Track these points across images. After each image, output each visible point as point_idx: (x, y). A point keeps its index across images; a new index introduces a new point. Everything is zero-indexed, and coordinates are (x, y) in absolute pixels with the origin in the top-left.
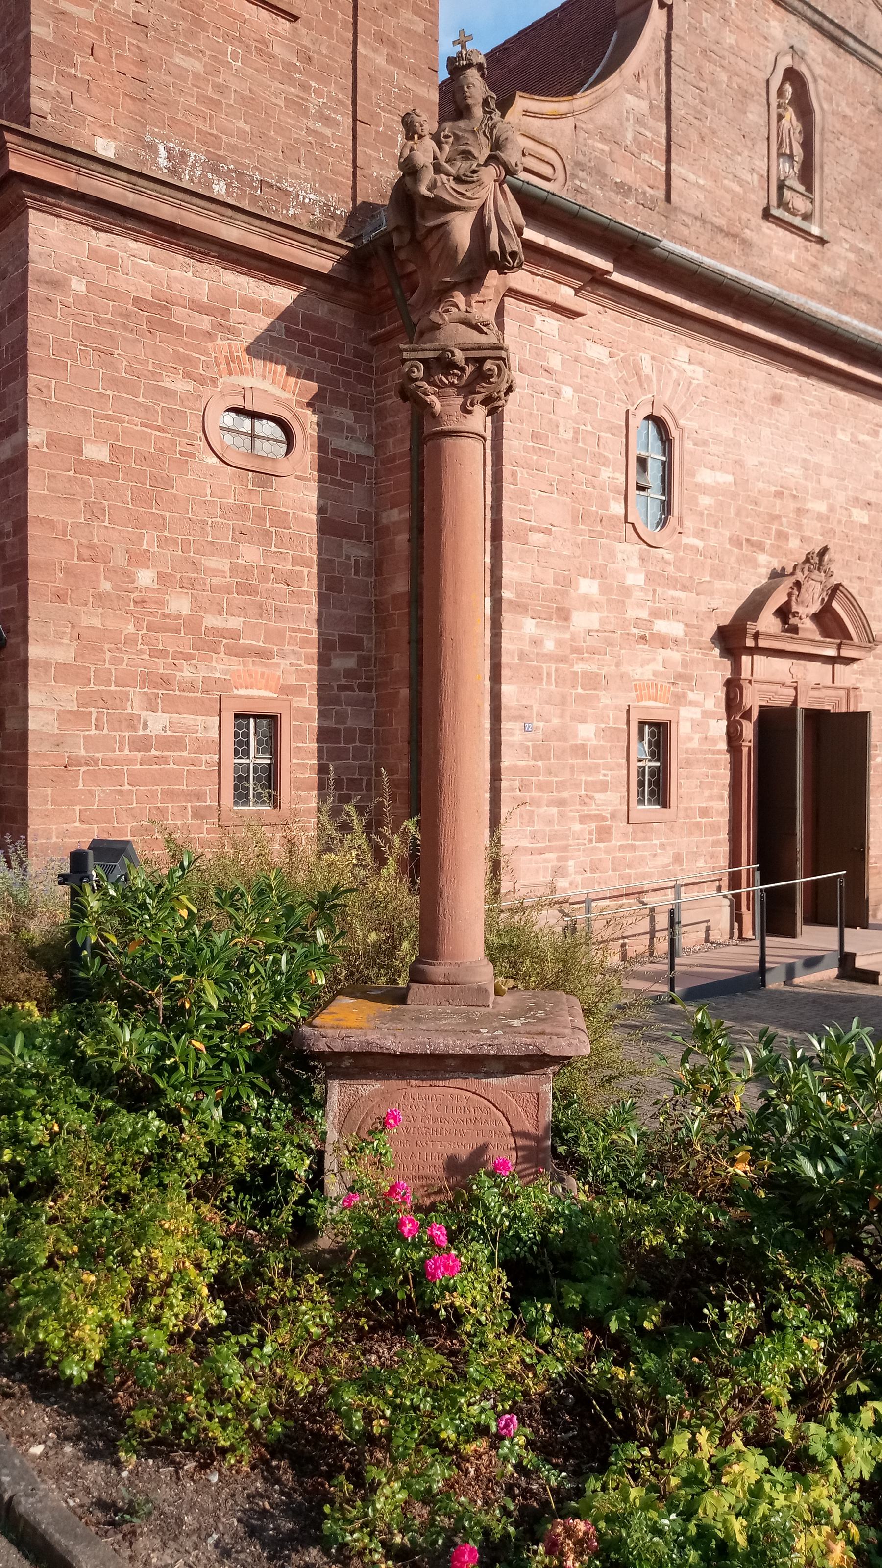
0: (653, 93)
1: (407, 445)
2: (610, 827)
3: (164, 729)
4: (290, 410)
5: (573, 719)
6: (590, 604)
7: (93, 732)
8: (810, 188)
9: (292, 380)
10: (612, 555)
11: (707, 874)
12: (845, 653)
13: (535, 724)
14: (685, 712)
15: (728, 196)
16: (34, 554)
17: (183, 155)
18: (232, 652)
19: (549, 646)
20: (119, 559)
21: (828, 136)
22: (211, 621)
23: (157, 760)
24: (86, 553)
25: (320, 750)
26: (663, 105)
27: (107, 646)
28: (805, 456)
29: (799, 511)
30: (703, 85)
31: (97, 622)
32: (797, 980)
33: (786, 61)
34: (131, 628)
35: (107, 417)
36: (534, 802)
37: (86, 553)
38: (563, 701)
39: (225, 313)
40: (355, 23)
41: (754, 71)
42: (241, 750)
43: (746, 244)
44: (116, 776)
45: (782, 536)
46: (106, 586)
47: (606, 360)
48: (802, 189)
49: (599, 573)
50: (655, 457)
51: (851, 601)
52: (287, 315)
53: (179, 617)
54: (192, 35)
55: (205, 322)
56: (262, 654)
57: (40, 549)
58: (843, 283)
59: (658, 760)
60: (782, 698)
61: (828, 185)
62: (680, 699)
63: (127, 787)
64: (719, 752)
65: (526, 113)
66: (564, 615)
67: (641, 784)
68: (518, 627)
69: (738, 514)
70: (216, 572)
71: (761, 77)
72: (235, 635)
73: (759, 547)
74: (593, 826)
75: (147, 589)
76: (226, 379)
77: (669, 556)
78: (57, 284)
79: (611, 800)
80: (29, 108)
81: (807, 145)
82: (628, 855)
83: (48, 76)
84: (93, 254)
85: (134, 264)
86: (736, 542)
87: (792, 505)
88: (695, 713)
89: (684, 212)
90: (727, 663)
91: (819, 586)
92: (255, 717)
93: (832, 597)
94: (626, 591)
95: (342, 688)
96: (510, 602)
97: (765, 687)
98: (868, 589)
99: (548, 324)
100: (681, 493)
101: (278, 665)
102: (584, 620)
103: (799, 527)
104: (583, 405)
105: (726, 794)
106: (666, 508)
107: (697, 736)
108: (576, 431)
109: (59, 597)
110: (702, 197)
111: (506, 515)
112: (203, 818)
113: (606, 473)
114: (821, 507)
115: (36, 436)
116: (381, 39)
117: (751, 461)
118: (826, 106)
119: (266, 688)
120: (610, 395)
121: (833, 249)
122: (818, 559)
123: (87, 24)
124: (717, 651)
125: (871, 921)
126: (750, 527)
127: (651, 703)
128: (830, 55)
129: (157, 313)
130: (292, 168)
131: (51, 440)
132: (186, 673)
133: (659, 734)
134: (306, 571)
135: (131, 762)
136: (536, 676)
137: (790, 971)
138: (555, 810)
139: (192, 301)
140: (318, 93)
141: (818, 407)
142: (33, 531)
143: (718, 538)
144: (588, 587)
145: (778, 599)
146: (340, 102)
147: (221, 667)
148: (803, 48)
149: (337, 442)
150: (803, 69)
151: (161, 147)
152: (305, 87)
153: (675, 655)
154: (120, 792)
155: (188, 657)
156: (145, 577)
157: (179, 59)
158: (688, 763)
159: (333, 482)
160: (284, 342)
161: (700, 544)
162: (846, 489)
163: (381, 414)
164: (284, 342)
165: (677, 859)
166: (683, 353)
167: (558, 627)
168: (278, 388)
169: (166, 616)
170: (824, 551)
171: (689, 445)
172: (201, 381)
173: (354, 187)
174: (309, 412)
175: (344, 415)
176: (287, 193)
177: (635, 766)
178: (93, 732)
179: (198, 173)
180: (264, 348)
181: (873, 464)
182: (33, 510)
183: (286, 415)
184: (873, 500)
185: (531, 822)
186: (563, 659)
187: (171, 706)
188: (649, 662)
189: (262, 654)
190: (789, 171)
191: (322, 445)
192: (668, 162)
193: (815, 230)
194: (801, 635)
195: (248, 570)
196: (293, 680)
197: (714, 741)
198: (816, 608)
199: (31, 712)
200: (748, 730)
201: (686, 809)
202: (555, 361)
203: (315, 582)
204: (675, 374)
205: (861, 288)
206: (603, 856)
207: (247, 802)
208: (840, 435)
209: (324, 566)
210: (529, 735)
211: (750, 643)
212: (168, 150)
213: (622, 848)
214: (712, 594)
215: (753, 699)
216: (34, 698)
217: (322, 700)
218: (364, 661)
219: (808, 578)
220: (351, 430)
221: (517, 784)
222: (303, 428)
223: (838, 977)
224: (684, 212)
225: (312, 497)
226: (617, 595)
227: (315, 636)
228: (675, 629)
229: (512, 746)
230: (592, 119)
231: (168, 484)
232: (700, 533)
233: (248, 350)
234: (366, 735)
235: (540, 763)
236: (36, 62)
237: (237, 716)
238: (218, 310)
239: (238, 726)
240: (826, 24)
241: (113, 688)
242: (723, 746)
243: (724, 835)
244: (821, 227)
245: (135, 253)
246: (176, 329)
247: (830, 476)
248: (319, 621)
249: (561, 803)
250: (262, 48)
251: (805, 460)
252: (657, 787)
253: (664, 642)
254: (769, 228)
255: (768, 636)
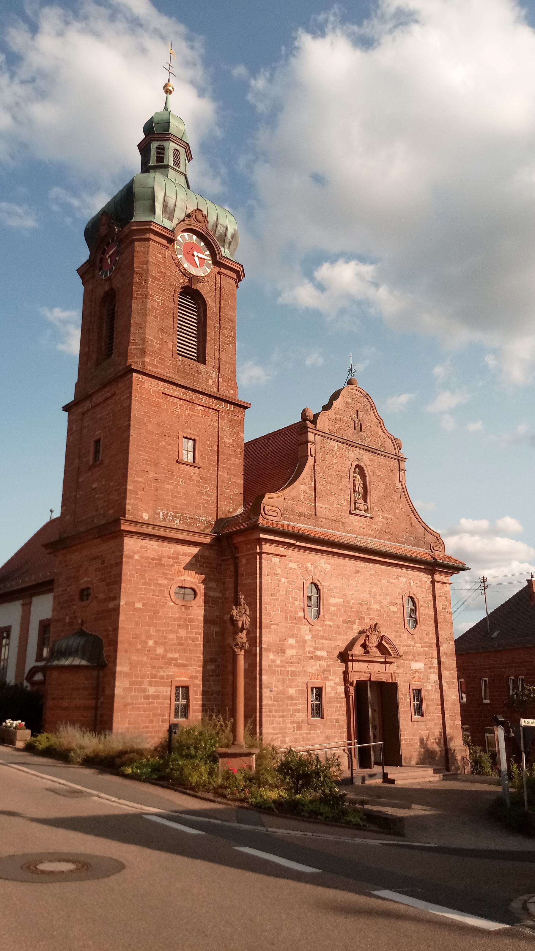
0: (310, 483)
1: (233, 595)
2: (302, 726)
3: (154, 692)
4: (196, 585)
5: (287, 687)
6: (292, 647)
7: (133, 694)
8: (366, 501)
9: (197, 575)
10: (299, 630)
11: (339, 744)
12: (388, 660)
13: (274, 689)
14: (327, 683)
15: (337, 510)
16: (120, 638)
17: (167, 514)
18: (175, 665)
19: (278, 662)
20: (144, 638)
21: (372, 483)
22: (170, 655)
23: (153, 703)
24: (134, 636)
25: (203, 698)
26: (313, 486)
27: (138, 666)
28: (370, 589)
29: (369, 609)
30: (326, 477)
31: (136, 658)
32: (366, 782)
33: (356, 463)
34: (145, 659)
35: (142, 594)
36: (274, 717)
37: (134, 636)
38: (284, 681)
39: (177, 558)
40: (218, 465)
41: (344, 469)
42: (177, 699)
43: (343, 523)
44: (139, 709)
45: (362, 618)
46: (139, 646)
47: (296, 567)
48: (363, 502)
49: (294, 636)
50: (314, 596)
51: (389, 641)
52: (196, 556)
53: (160, 655)
54: (170, 479)
55: (171, 562)
56: (185, 665)
57: (122, 637)
58: (381, 530)
59: (319, 701)
60: (365, 677)
61: (373, 500)
62: (326, 679)
63: (142, 712)
64: (342, 698)
65: (269, 498)
66: (283, 652)
67: (313, 710)
68: (268, 656)
69: (345, 612)
70: (172, 639)
71: (346, 470)
72: (176, 659)
73: (354, 623)
74: (295, 725)
75: (151, 646)
76: (177, 578)
77: (320, 628)
78: (131, 557)
79: (301, 716)
80: (125, 508)
81: (365, 488)
82: (309, 736)
83: (131, 499)
84: (141, 547)
85: (153, 548)
86: (345, 622)
87: (366, 607)
88: (332, 684)
89: (321, 517)
90: (344, 665)
91: (376, 637)
92: (182, 687)
93: (382, 640)
94: (305, 642)
95: (210, 676)
96: (265, 648)
97: (358, 673)
98: (398, 635)
99: (276, 560)
100: (323, 608)
101: (189, 669)
102: (290, 653)
103: (369, 614)
104: (288, 582)
105: (345, 713)
106: (319, 612)
107: (333, 692)
108: (286, 591)
109: (126, 651)
110: (327, 512)
111: (263, 620)
112: (164, 723)
113: (297, 603)
114: (377, 607)
115: (122, 603)
116: (225, 468)
117: (349, 593)
118: (371, 474)
119: (186, 677)
120: (298, 578)
121: (376, 519)
122: (374, 627)
123: (142, 483)
124: (339, 661)
125: (404, 763)
126: (350, 616)
127: (315, 680)
128: (371, 457)
129: (158, 562)
130: (198, 511)
131: (127, 603)
132: (161, 673)
133: (319, 692)
134: (199, 636)
135: (143, 703)
136: (274, 673)
137: (363, 779)
138: (281, 719)
139: (168, 556)
140: (206, 488)
141: (373, 572)
142: (120, 631)
143: (338, 621)
144: (292, 641)
145: (361, 641)
146: (213, 489)
147: (172, 670)
148: (362, 458)
149: (211, 594)
150: (362, 464)
151: (161, 513)
152: (203, 487)
153: (324, 663)
154: (140, 714)
155: (162, 668)
156: (151, 643)
157: (167, 486)
158: (330, 702)
159: (209, 607)
160: (195, 565)
161: (331, 624)
162: (387, 599)
163: (224, 583)
164: (195, 565)
165: (327, 738)
166: (322, 561)
167: (281, 656)
168: (193, 579)
169: (156, 655)
170: (376, 624)
171: (326, 590)
172: (170, 579)
173: (217, 514)
174: (202, 585)
175: (213, 585)
176: (197, 519)
177: (310, 703)
178: (133, 694)
179: (171, 518)
180: (189, 567)
181: (397, 590)
182: (120, 625)
183: (194, 587)
184: (398, 602)
185: (273, 724)
186: (283, 666)
187: (157, 684)
188: (314, 666)
189: (185, 665)
190: (359, 497)
191: (206, 595)
192: (315, 503)
193: (368, 515)
194: (371, 654)
195: (181, 638)
196: (194, 674)
197: (340, 694)
198: (376, 643)
199: (116, 688)
200: (352, 690)
201: (330, 719)
202: (279, 571)
203: (202, 640)
204: (320, 568)
205: (388, 530)
206: (299, 736)
207: (178, 718)
208: (383, 581)
209: (205, 634)
210: (272, 693)
211: (350, 658)
212: (163, 513)
213: (306, 733)
214: (337, 641)
215: (353, 678)
216: (117, 683)
217: (204, 681)
218: (218, 666)
219: (371, 634)
220: (215, 589)
221: (268, 710)
222: (200, 590)
223: (383, 782)
224: (321, 517)
225: (202, 612)
226: (302, 643)
227: (202, 658)
228: (323, 654)
229: (266, 697)
230: (290, 495)
231: (158, 612)
232: (331, 620)
233: (184, 568)
234: (218, 692)
235: (276, 703)
236: (128, 496)
237: (176, 687)
238: (175, 557)
239: (176, 690)
240: (369, 449)
241: (140, 679)
242: (343, 695)
243: (345, 729)
244: (371, 513)
245: (153, 544)
246: (163, 565)
247: (380, 595)
248: (203, 653)
249: (283, 717)
250: (190, 478)
251: (370, 591)
252: (318, 711)
253: (319, 658)
254: (352, 517)
255: (357, 655)
